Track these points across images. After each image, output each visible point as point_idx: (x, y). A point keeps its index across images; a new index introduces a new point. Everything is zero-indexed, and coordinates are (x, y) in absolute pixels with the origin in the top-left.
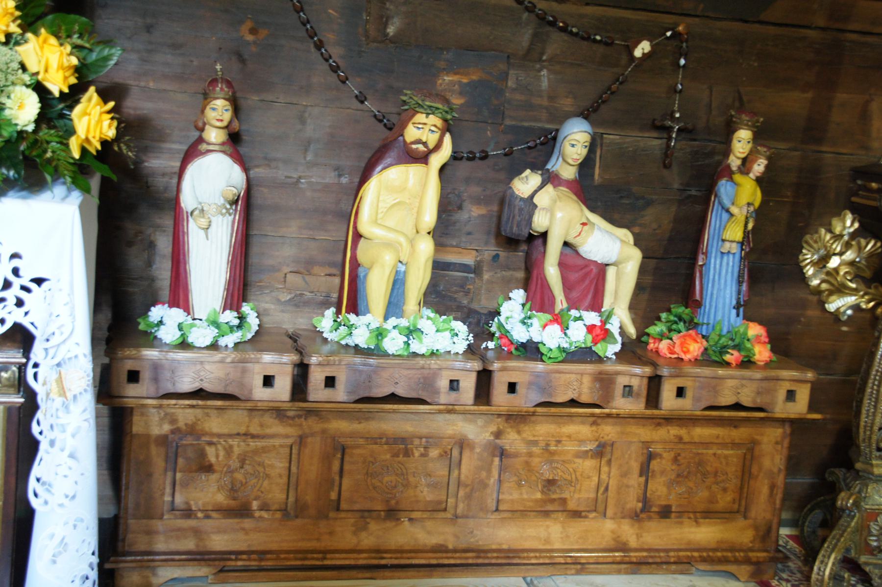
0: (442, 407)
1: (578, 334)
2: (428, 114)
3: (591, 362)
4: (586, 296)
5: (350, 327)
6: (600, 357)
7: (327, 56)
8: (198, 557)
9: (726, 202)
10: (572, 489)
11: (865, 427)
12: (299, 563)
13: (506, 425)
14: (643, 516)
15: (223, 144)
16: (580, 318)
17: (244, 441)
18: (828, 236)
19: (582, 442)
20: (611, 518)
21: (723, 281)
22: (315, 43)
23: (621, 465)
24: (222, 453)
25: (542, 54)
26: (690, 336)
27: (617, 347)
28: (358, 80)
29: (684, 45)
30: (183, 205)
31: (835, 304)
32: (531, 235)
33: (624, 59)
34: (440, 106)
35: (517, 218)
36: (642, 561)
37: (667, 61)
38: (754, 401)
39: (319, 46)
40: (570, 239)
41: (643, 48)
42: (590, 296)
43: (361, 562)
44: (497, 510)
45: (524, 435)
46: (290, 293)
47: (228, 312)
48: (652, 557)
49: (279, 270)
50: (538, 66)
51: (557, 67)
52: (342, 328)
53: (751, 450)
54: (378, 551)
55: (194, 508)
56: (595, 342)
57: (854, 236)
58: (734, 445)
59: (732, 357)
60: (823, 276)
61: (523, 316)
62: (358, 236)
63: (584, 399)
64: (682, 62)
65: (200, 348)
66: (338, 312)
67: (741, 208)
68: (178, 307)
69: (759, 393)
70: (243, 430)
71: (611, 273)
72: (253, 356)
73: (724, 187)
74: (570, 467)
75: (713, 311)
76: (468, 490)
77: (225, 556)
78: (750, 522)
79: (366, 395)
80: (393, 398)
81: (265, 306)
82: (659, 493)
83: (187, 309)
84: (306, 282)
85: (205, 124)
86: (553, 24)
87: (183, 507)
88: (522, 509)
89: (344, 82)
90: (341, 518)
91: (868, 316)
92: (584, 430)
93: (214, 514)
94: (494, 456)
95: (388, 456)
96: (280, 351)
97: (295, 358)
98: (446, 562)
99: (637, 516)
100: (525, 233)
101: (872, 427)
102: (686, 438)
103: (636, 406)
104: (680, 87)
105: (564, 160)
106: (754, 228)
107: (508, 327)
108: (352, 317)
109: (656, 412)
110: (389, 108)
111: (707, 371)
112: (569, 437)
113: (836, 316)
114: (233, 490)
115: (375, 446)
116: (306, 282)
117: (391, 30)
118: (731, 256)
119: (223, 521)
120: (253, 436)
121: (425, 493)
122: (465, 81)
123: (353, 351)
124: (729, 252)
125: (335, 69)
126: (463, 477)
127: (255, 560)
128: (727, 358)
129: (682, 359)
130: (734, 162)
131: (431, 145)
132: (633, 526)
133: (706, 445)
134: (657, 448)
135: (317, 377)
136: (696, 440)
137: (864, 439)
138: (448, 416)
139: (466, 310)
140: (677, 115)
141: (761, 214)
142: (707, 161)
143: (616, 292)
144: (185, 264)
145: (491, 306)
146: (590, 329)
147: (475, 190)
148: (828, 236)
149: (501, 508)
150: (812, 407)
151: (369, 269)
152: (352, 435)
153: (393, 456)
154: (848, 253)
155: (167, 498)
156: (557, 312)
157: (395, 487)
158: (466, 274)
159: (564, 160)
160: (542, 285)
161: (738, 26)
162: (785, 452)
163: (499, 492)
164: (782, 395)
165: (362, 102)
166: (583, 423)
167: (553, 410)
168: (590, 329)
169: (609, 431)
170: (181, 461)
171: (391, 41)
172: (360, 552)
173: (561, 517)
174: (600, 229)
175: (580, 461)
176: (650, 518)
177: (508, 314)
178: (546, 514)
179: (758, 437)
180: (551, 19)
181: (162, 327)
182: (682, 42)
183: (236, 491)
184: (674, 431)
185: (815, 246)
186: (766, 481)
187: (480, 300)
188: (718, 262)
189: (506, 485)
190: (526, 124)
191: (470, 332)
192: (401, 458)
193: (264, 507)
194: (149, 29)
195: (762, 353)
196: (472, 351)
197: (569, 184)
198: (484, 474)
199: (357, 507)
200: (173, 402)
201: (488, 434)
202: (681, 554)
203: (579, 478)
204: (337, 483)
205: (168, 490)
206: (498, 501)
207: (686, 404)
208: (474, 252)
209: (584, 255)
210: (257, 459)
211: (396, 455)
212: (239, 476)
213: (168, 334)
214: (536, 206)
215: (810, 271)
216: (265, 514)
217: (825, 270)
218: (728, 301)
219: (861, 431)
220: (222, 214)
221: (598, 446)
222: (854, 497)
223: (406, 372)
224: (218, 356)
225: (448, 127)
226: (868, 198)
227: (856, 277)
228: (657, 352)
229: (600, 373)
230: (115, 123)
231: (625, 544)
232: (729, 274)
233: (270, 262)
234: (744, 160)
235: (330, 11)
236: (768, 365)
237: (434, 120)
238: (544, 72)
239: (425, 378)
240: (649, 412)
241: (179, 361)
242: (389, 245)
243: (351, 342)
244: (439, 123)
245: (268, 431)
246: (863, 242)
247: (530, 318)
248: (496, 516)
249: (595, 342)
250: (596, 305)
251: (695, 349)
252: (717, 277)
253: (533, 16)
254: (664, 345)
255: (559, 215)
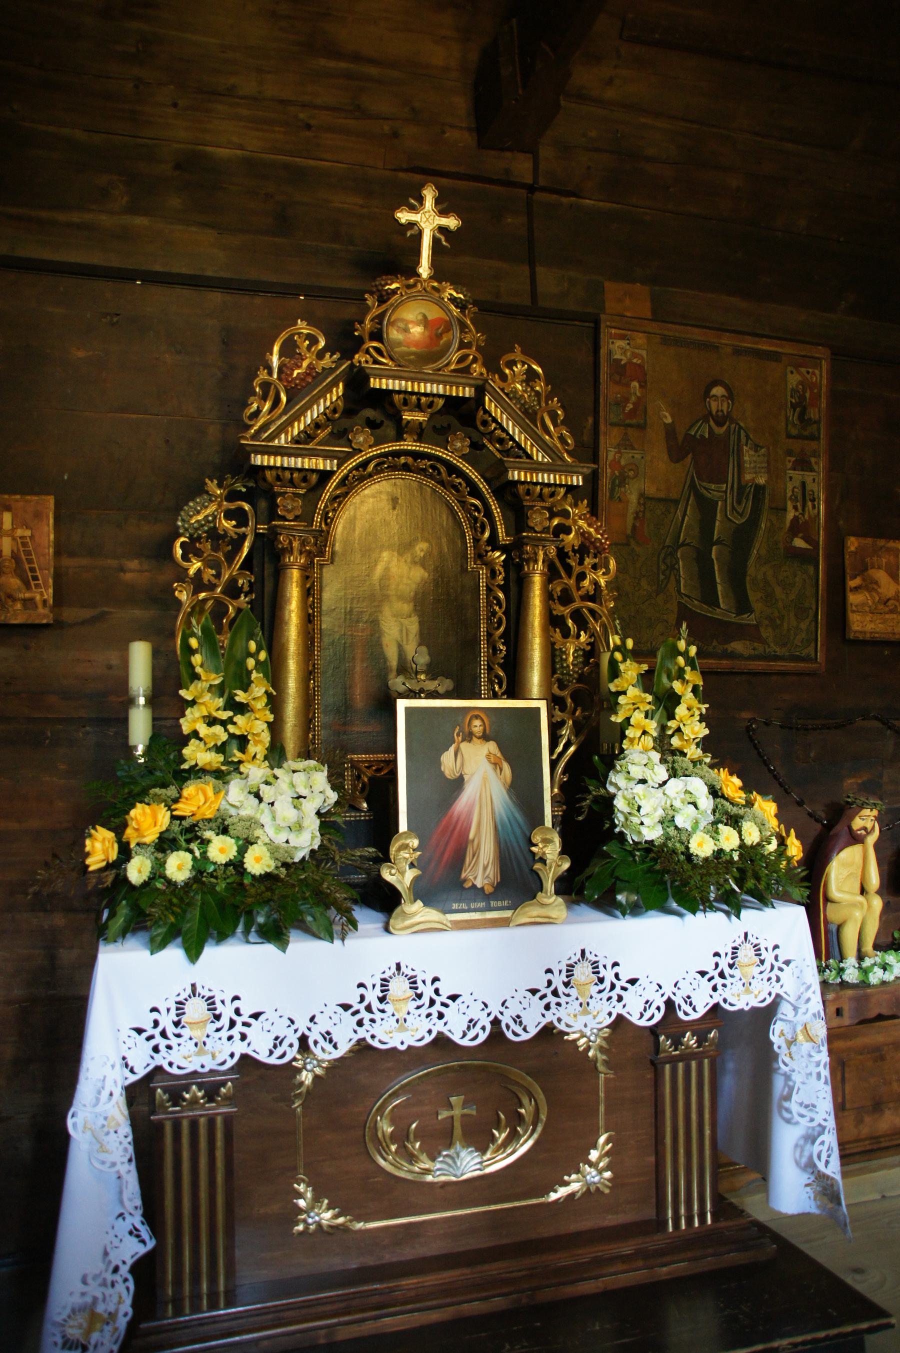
80: (880, 1018)
122: (860, 781)
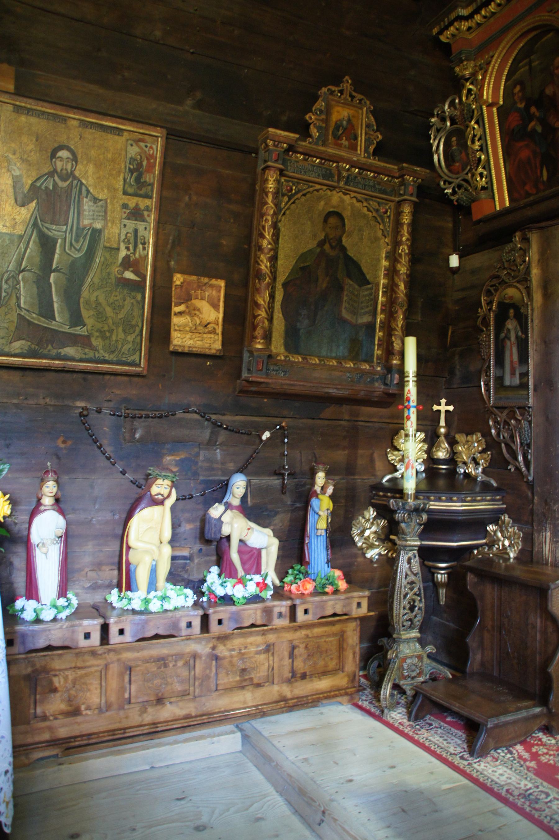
0: (183, 638)
1: (252, 589)
2: (164, 480)
3: (259, 602)
4: (253, 567)
5: (130, 599)
6: (263, 599)
7: (104, 452)
8: (52, 743)
9: (317, 509)
10: (255, 672)
11: (396, 616)
12: (111, 738)
13: (218, 642)
14: (293, 680)
15: (53, 505)
16: (252, 580)
17: (74, 671)
18: (363, 521)
19: (258, 646)
20: (277, 684)
21: (319, 550)
22: (97, 446)
23: (279, 655)
24: (62, 680)
25: (216, 442)
26: (307, 581)
27: (272, 592)
28: (121, 463)
29: (286, 432)
30: (32, 541)
31: (372, 554)
32: (221, 538)
33: (257, 441)
34: (170, 475)
35: (214, 530)
36: (296, 704)
37: (278, 440)
38: (342, 611)
39: (100, 447)
40: (243, 538)
41: (266, 435)
42: (255, 567)
43: (145, 731)
44: (217, 690)
45: (228, 646)
46: (90, 582)
47: (61, 599)
48: (300, 701)
49: (83, 570)
50: (215, 448)
51: (224, 448)
52: (124, 600)
53: (342, 636)
54: (154, 724)
55: (48, 715)
56: (261, 591)
57: (374, 519)
58: (334, 635)
59: (329, 589)
60: (363, 541)
61: (221, 581)
62: (129, 548)
63: (259, 622)
64: (286, 440)
65: (47, 622)
66: (120, 591)
67: (324, 511)
68: (32, 599)
69: (344, 606)
70: (73, 665)
71: (264, 553)
72: (78, 623)
73: (314, 502)
74: (253, 660)
75: (316, 566)
76: (200, 681)
77: (68, 740)
78: (345, 673)
79: (141, 637)
81: (77, 591)
82: (299, 667)
83: (38, 600)
84: (99, 576)
85: (42, 495)
86: (221, 426)
87: (41, 715)
88: (230, 687)
89: (114, 465)
90: (132, 708)
91: (385, 557)
92: (259, 639)
93: (60, 717)
94: (213, 660)
95: (155, 669)
96: (93, 618)
97: (101, 621)
98: (192, 723)
99: (290, 680)
100: (218, 537)
101: (399, 615)
102: (310, 635)
103: (285, 622)
104: (286, 452)
105: (233, 496)
106: (331, 520)
107: (213, 588)
108: (129, 593)
109: (295, 624)
110: (140, 477)
111: (317, 599)
112: (251, 644)
113: (371, 560)
114: (70, 700)
115: (148, 664)
116: (99, 576)
117: (137, 436)
118: (322, 537)
119: (65, 719)
120: (79, 668)
121: (177, 687)
122: (178, 458)
123: (131, 613)
124: (321, 535)
125: (108, 458)
126: (197, 675)
127: (85, 740)
128: (327, 590)
129: (304, 594)
130: (318, 488)
131: (165, 496)
132: (288, 686)
133: (320, 637)
134: (296, 643)
135: (114, 630)
136: (315, 635)
137: (396, 623)
138: (186, 642)
139: (187, 581)
140: (287, 467)
141: (333, 514)
142: (303, 489)
143: (267, 563)
144: (35, 574)
145: (201, 577)
146: (258, 584)
147: (187, 515)
148: (363, 521)
149: (219, 688)
150: (369, 610)
151: (137, 566)
152: (135, 660)
153: (158, 668)
154: (373, 527)
155: (32, 711)
156: (239, 577)
157: (160, 686)
158: (185, 561)
159: (233, 496)
160: (230, 565)
161: (310, 421)
162: (358, 634)
163: (217, 680)
164: (355, 605)
165: (124, 475)
166: (257, 635)
167: (243, 630)
168: (258, 584)
169: (271, 638)
170: (39, 689)
171: (138, 441)
172: (145, 725)
173: (251, 688)
174: (256, 530)
175: (257, 656)
176: (296, 681)
177: (212, 581)
178: (243, 688)
179: (344, 629)
180: (219, 424)
181: (25, 612)
182: (285, 431)
183: (71, 701)
184: (304, 632)
185: (358, 526)
186: (351, 651)
187: (194, 574)
188: (316, 540)
189: (220, 676)
190: (211, 478)
191: (194, 593)
192: (162, 669)
193: (88, 708)
194: (8, 446)
195: (342, 585)
196: (196, 604)
197: (237, 508)
198: (208, 671)
199: (140, 700)
200: (34, 655)
201: (208, 649)
202: (314, 697)
203: (258, 665)
204: (128, 688)
205: (32, 706)
206: (217, 685)
207: (309, 617)
208: (188, 549)
209: (250, 545)
210: (83, 681)
211: (159, 668)
212: (73, 692)
213: (28, 616)
214: (222, 522)
215: (357, 539)
216: (89, 712)
217: (364, 537)
218: (323, 560)
219: (394, 618)
220: (55, 544)
221: (267, 646)
222: (395, 653)
223: (163, 621)
224: (58, 625)
225: (174, 485)
226: (379, 500)
227: (379, 539)
228: (290, 591)
229: (265, 607)
230: (11, 506)
231: (285, 697)
232: (322, 546)
233: (77, 566)
234: (322, 488)
235: (105, 428)
236: (346, 591)
237: (167, 482)
238: (218, 451)
239: (174, 623)
240: (292, 624)
241: (36, 631)
242: (146, 551)
243: (130, 607)
244: (169, 483)
245: (88, 664)
246: (379, 521)
247: (225, 582)
248: (217, 693)
249: (261, 591)
250: (258, 572)
251: (310, 587)
252: (316, 548)
253: (210, 423)
254: (294, 587)
255: (236, 526)
